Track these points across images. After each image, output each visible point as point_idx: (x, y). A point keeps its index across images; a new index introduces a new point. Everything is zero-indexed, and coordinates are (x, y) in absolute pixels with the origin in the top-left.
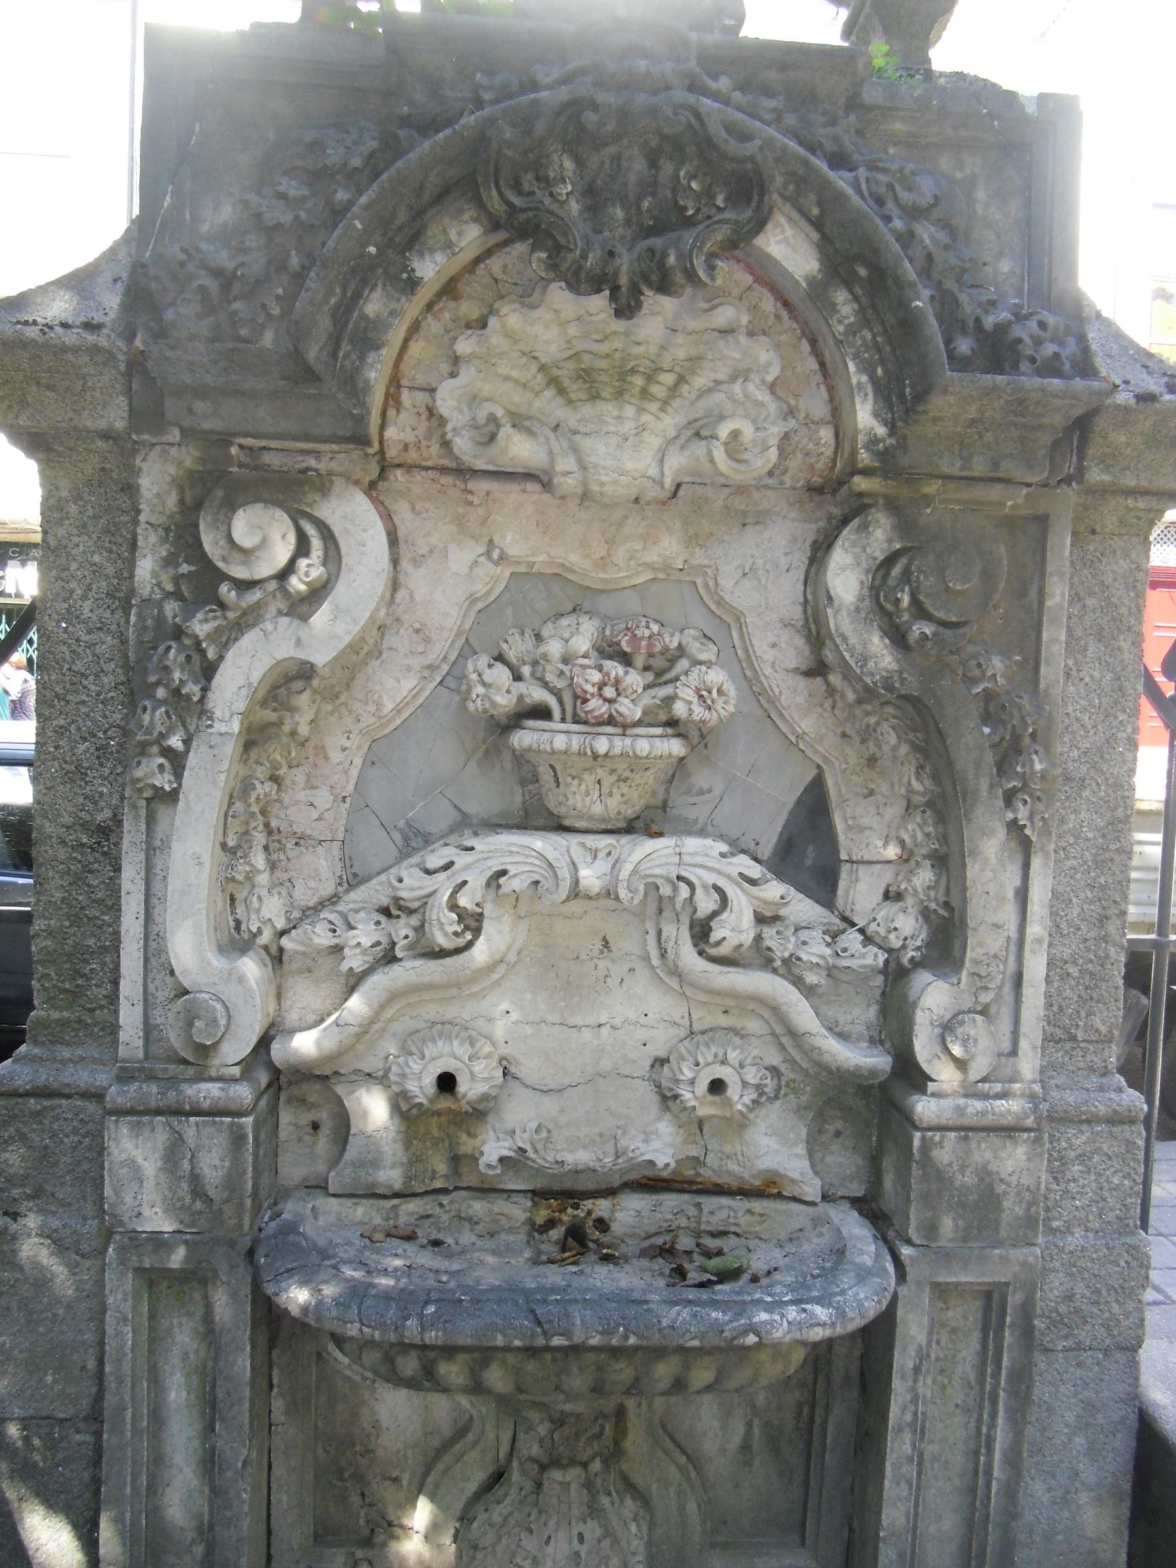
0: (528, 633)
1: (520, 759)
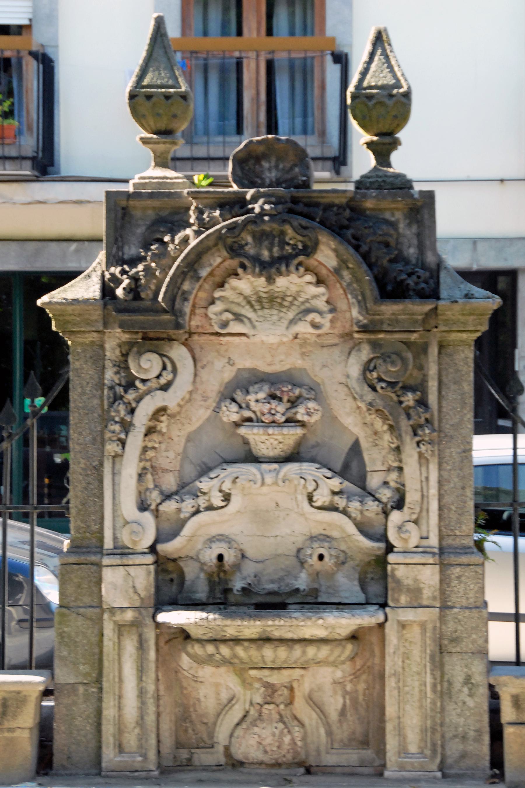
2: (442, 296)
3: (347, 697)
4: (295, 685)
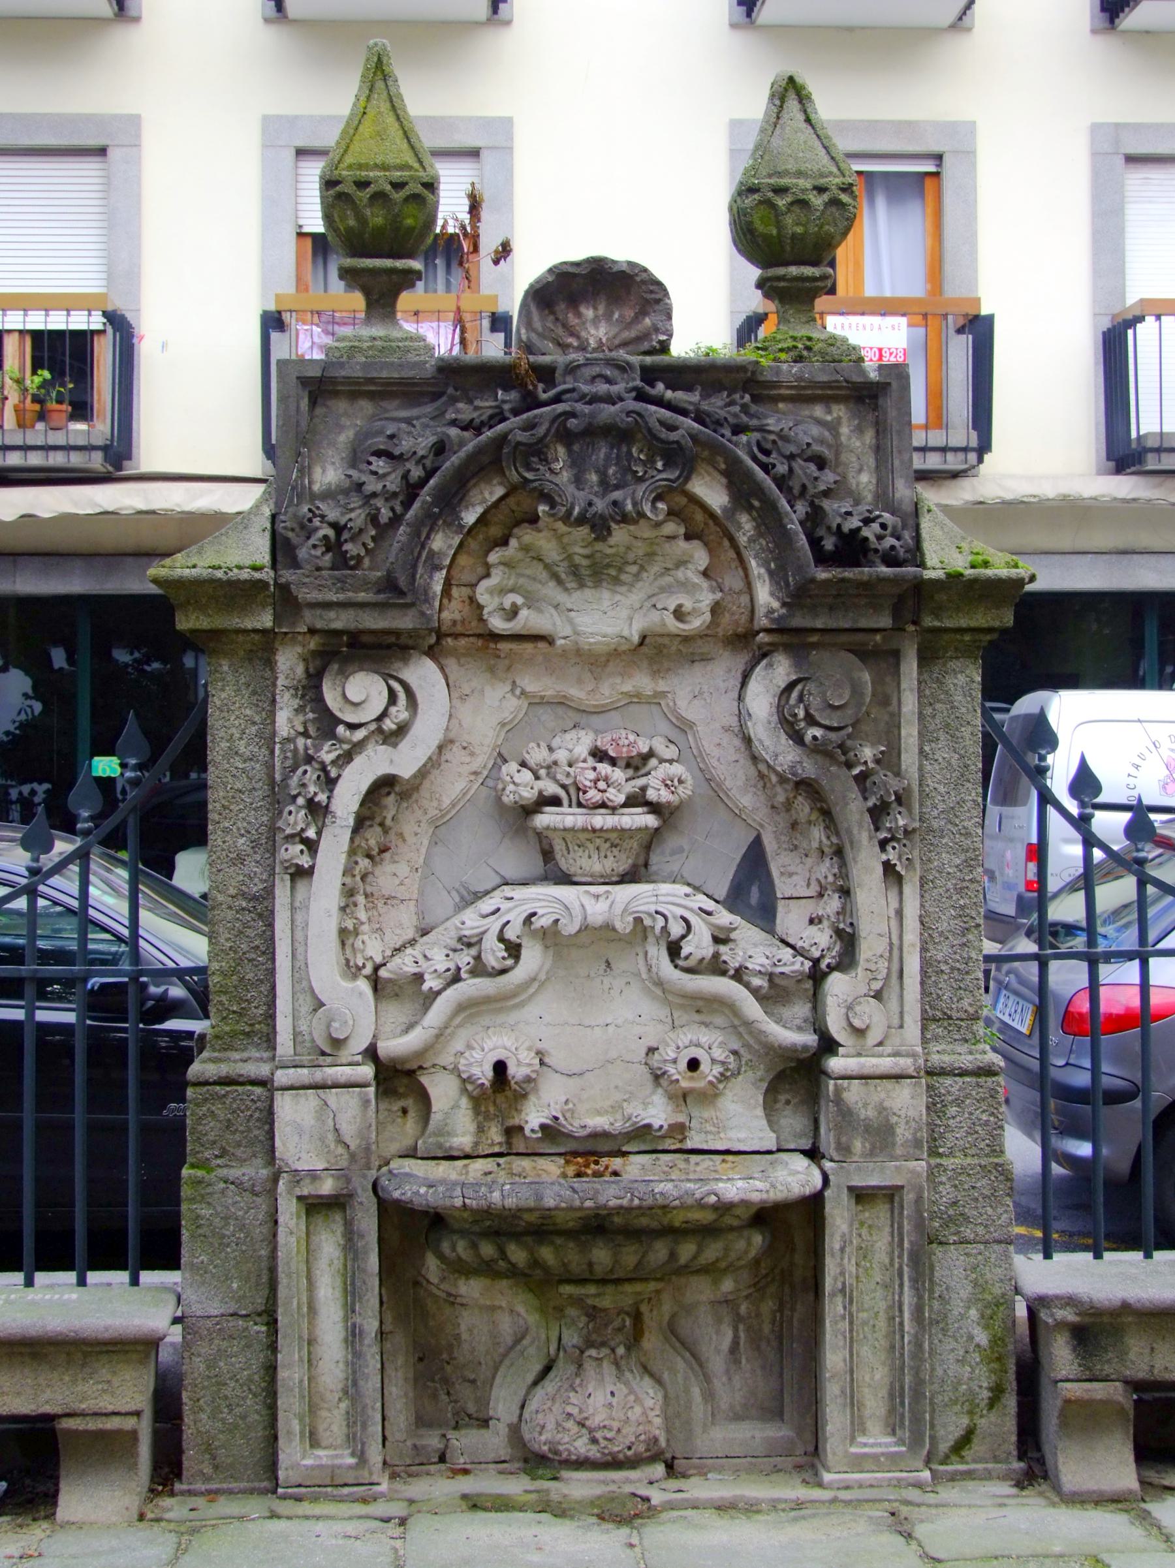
0: (543, 745)
1: (539, 835)
2: (929, 563)
3: (741, 1327)
4: (644, 1308)
